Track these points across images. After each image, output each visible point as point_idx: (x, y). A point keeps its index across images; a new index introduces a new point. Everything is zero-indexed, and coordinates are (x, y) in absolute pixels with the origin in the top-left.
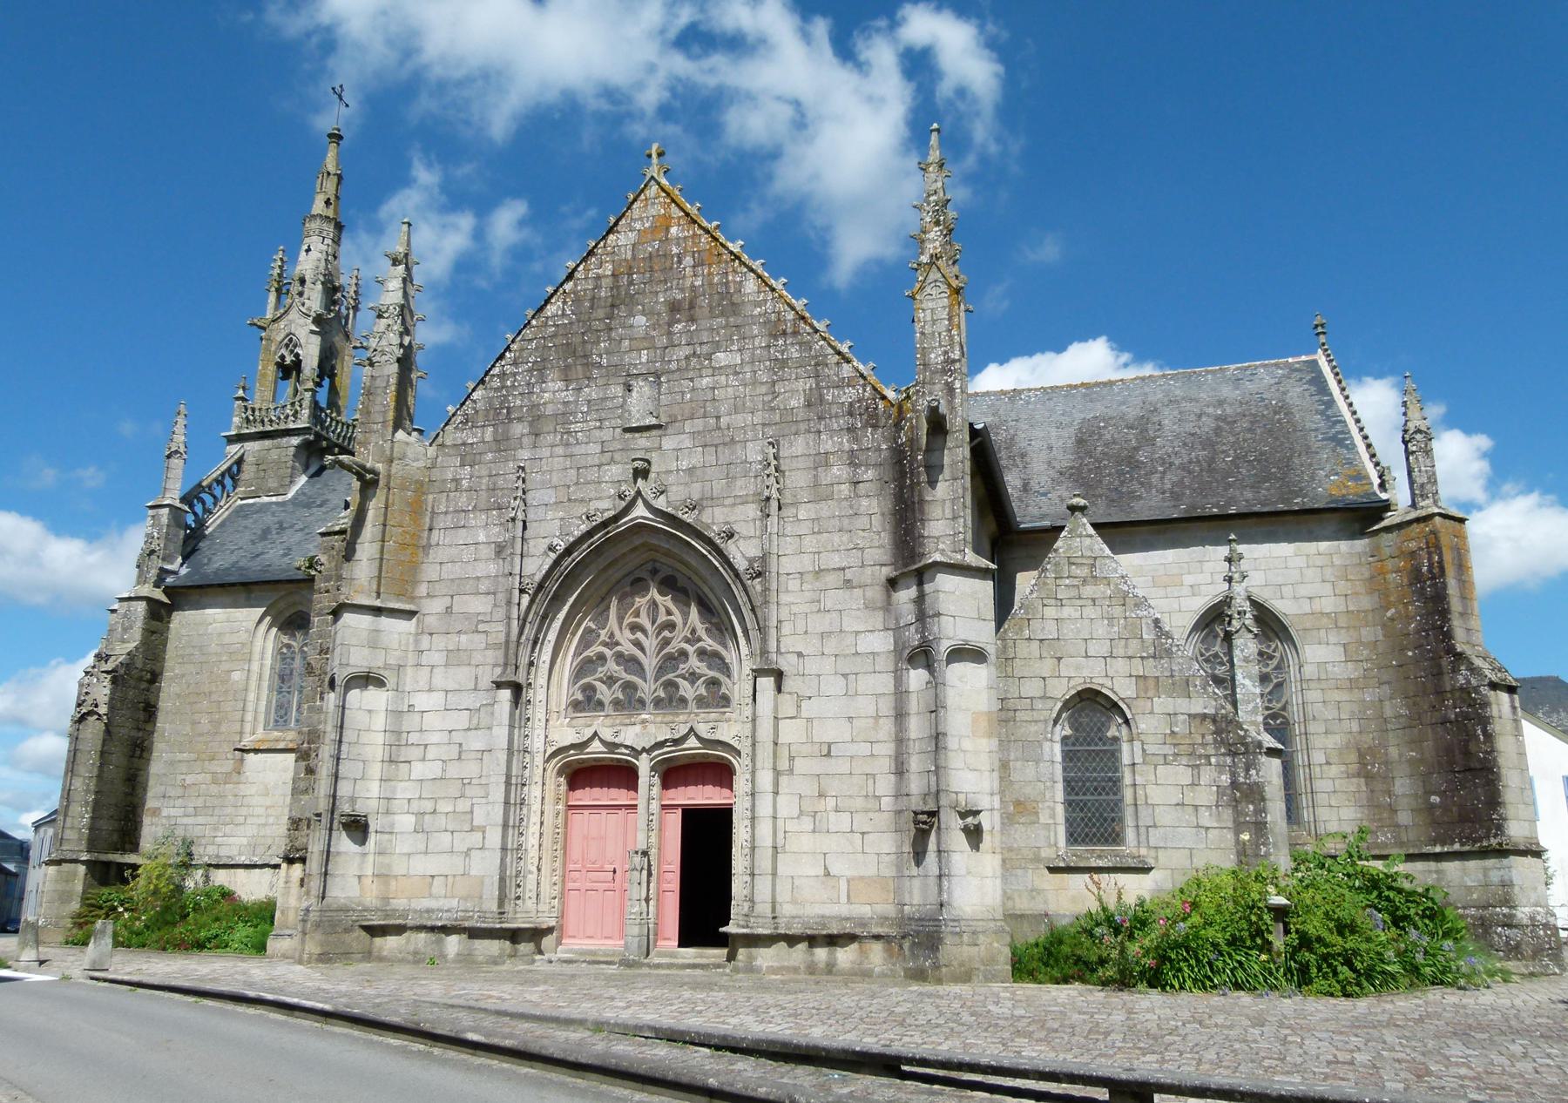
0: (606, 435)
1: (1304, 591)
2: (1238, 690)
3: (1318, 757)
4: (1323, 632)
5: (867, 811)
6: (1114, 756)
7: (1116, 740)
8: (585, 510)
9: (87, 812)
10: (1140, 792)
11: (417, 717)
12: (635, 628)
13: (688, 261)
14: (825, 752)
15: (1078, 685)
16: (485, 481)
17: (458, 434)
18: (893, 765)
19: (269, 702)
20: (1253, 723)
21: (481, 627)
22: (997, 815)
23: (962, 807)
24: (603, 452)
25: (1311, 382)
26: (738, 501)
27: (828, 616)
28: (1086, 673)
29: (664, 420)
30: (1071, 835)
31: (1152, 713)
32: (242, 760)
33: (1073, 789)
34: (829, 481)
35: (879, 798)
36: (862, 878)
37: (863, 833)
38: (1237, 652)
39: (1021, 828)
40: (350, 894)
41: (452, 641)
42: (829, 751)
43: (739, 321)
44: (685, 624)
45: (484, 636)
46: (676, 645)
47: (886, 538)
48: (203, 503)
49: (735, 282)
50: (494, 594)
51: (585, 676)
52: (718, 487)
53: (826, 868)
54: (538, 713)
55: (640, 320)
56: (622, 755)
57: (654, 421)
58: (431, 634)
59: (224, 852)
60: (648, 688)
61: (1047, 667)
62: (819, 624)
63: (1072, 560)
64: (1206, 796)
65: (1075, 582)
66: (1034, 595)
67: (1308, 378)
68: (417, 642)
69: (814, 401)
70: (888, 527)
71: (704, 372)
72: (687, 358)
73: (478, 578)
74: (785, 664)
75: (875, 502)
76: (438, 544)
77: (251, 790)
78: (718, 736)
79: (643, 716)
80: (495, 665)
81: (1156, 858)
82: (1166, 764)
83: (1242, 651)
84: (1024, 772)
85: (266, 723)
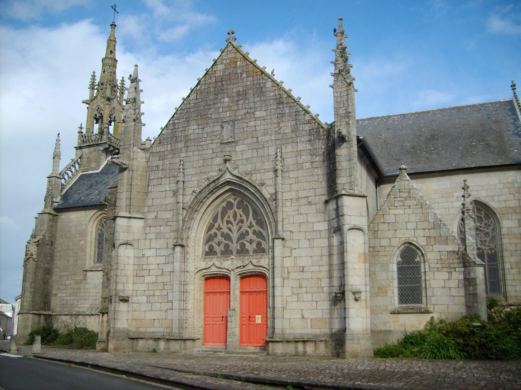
0: (214, 146)
1: (502, 198)
2: (467, 241)
3: (507, 266)
4: (510, 215)
5: (318, 293)
6: (418, 268)
7: (419, 263)
8: (207, 176)
9: (31, 295)
10: (428, 283)
11: (146, 259)
12: (228, 222)
13: (244, 75)
14: (301, 270)
15: (403, 240)
16: (168, 166)
17: (158, 148)
18: (328, 274)
19: (95, 252)
20: (473, 254)
21: (168, 224)
22: (368, 294)
23: (354, 290)
24: (213, 153)
25: (509, 110)
26: (266, 171)
27: (302, 216)
28: (406, 236)
29: (236, 139)
30: (401, 300)
31: (433, 251)
32: (86, 275)
33: (402, 282)
34: (301, 162)
35: (323, 288)
36: (316, 319)
37: (317, 302)
38: (466, 226)
39: (380, 298)
40: (124, 327)
41: (157, 230)
42: (303, 269)
43: (265, 98)
44: (247, 220)
45: (169, 227)
46: (245, 228)
47: (324, 184)
48: (68, 175)
49: (263, 83)
50: (173, 210)
51: (209, 242)
52: (258, 165)
53: (302, 315)
54: (190, 257)
55: (226, 100)
56: (224, 272)
57: (233, 140)
58: (150, 227)
59: (81, 310)
60: (234, 246)
61: (390, 234)
62: (299, 219)
63: (401, 190)
64: (454, 283)
65: (402, 199)
66: (386, 205)
67: (508, 108)
68: (145, 230)
69: (295, 130)
70: (325, 180)
71: (252, 120)
72: (245, 114)
73: (167, 204)
74: (286, 235)
75: (320, 170)
76: (151, 192)
77: (90, 286)
78: (260, 264)
79: (232, 257)
80: (174, 238)
81: (434, 309)
82: (438, 271)
83: (468, 225)
84: (381, 276)
85: (94, 260)
